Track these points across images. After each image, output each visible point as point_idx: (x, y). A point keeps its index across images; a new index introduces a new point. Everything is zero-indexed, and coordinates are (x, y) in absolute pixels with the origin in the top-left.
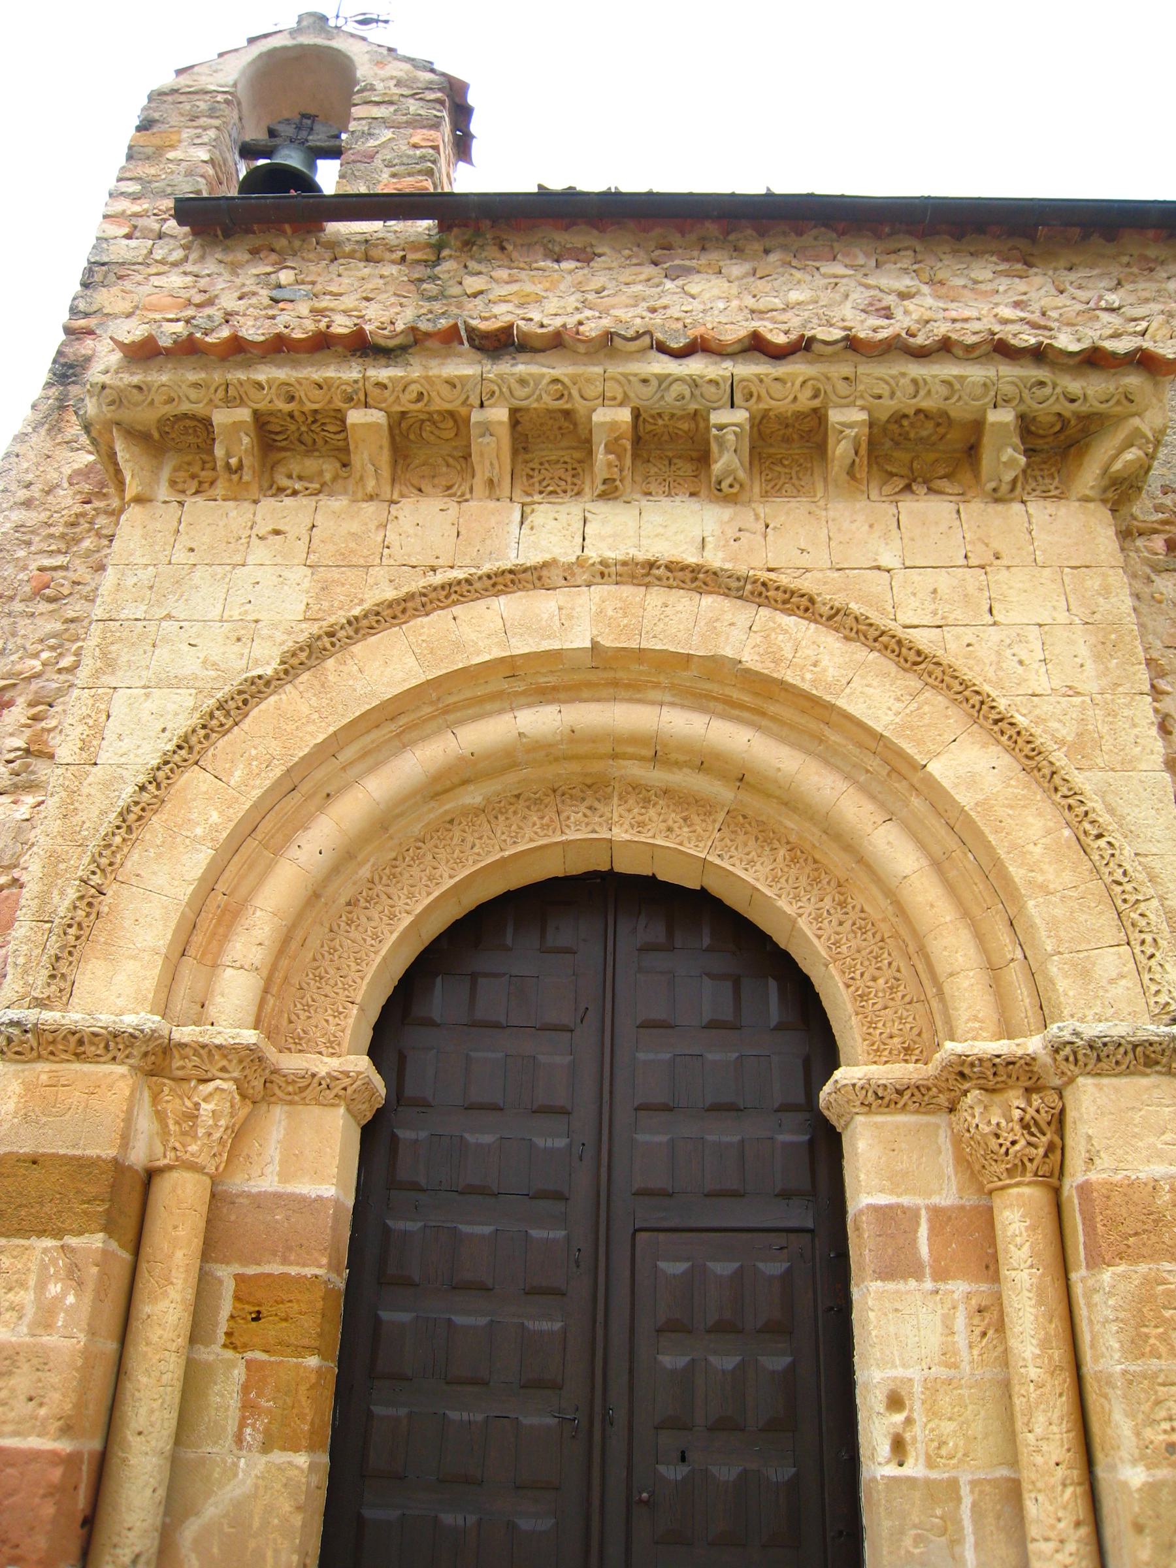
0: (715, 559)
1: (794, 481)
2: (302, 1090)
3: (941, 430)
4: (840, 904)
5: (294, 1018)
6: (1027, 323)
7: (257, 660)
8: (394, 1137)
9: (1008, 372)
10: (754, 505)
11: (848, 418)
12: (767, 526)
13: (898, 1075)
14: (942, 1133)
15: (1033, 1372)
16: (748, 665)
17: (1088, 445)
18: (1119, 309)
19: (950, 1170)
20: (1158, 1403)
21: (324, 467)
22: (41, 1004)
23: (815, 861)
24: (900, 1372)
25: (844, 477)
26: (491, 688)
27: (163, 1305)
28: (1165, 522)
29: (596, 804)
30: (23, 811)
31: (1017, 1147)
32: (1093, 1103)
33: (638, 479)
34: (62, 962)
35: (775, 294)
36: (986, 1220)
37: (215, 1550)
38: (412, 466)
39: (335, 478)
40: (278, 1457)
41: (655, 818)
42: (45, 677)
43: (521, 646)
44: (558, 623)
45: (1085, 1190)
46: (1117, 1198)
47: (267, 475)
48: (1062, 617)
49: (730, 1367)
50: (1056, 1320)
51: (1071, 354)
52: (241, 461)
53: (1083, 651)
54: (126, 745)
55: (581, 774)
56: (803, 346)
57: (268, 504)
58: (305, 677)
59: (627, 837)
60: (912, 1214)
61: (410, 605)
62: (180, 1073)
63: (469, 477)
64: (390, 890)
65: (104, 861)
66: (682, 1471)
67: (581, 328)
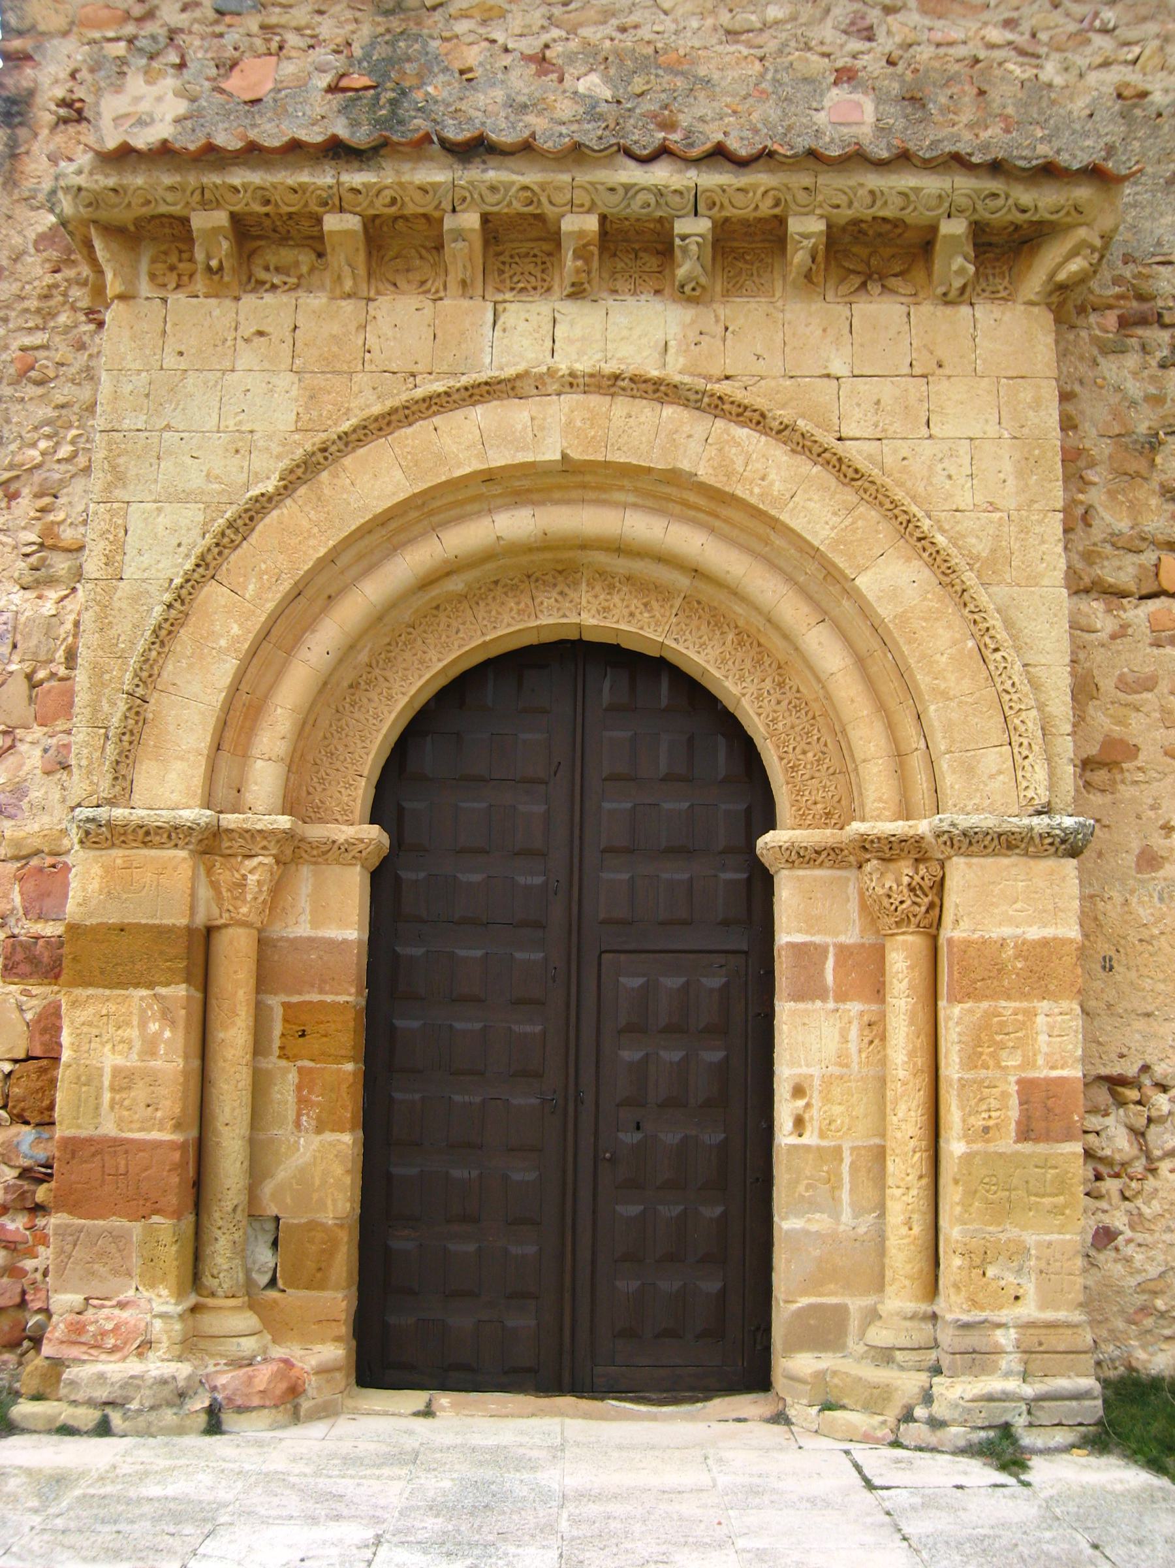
0: (675, 369)
1: (755, 278)
2: (325, 853)
3: (899, 231)
4: (779, 684)
5: (311, 790)
6: (1015, 49)
7: (256, 473)
8: (398, 879)
9: (964, 184)
10: (715, 306)
11: (807, 227)
12: (727, 329)
13: (817, 839)
14: (851, 884)
15: (901, 1074)
16: (702, 479)
17: (1039, 246)
18: (1114, 29)
19: (856, 915)
20: (981, 1100)
21: (301, 258)
22: (112, 802)
23: (759, 645)
24: (804, 1070)
25: (803, 280)
26: (471, 492)
27: (232, 1032)
28: (1120, 297)
29: (566, 590)
30: (48, 608)
31: (904, 906)
32: (962, 874)
33: (605, 275)
34: (122, 766)
35: (752, 8)
36: (878, 955)
37: (289, 1200)
38: (386, 259)
39: (312, 270)
40: (329, 1136)
41: (619, 604)
42: (45, 468)
43: (499, 458)
44: (531, 435)
45: (950, 941)
46: (972, 952)
47: (245, 267)
48: (992, 430)
49: (677, 1059)
50: (923, 1037)
51: (1024, 169)
52: (221, 262)
53: (1008, 467)
54: (146, 559)
55: (555, 564)
56: (765, 157)
57: (249, 301)
58: (302, 490)
59: (594, 622)
60: (822, 950)
61: (393, 418)
62: (229, 852)
63: (442, 273)
64: (388, 674)
65: (144, 674)
66: (638, 1136)
67: (548, 53)
